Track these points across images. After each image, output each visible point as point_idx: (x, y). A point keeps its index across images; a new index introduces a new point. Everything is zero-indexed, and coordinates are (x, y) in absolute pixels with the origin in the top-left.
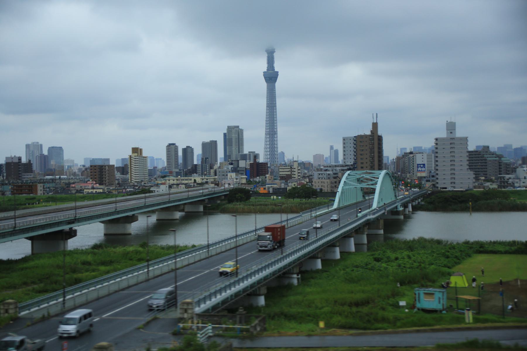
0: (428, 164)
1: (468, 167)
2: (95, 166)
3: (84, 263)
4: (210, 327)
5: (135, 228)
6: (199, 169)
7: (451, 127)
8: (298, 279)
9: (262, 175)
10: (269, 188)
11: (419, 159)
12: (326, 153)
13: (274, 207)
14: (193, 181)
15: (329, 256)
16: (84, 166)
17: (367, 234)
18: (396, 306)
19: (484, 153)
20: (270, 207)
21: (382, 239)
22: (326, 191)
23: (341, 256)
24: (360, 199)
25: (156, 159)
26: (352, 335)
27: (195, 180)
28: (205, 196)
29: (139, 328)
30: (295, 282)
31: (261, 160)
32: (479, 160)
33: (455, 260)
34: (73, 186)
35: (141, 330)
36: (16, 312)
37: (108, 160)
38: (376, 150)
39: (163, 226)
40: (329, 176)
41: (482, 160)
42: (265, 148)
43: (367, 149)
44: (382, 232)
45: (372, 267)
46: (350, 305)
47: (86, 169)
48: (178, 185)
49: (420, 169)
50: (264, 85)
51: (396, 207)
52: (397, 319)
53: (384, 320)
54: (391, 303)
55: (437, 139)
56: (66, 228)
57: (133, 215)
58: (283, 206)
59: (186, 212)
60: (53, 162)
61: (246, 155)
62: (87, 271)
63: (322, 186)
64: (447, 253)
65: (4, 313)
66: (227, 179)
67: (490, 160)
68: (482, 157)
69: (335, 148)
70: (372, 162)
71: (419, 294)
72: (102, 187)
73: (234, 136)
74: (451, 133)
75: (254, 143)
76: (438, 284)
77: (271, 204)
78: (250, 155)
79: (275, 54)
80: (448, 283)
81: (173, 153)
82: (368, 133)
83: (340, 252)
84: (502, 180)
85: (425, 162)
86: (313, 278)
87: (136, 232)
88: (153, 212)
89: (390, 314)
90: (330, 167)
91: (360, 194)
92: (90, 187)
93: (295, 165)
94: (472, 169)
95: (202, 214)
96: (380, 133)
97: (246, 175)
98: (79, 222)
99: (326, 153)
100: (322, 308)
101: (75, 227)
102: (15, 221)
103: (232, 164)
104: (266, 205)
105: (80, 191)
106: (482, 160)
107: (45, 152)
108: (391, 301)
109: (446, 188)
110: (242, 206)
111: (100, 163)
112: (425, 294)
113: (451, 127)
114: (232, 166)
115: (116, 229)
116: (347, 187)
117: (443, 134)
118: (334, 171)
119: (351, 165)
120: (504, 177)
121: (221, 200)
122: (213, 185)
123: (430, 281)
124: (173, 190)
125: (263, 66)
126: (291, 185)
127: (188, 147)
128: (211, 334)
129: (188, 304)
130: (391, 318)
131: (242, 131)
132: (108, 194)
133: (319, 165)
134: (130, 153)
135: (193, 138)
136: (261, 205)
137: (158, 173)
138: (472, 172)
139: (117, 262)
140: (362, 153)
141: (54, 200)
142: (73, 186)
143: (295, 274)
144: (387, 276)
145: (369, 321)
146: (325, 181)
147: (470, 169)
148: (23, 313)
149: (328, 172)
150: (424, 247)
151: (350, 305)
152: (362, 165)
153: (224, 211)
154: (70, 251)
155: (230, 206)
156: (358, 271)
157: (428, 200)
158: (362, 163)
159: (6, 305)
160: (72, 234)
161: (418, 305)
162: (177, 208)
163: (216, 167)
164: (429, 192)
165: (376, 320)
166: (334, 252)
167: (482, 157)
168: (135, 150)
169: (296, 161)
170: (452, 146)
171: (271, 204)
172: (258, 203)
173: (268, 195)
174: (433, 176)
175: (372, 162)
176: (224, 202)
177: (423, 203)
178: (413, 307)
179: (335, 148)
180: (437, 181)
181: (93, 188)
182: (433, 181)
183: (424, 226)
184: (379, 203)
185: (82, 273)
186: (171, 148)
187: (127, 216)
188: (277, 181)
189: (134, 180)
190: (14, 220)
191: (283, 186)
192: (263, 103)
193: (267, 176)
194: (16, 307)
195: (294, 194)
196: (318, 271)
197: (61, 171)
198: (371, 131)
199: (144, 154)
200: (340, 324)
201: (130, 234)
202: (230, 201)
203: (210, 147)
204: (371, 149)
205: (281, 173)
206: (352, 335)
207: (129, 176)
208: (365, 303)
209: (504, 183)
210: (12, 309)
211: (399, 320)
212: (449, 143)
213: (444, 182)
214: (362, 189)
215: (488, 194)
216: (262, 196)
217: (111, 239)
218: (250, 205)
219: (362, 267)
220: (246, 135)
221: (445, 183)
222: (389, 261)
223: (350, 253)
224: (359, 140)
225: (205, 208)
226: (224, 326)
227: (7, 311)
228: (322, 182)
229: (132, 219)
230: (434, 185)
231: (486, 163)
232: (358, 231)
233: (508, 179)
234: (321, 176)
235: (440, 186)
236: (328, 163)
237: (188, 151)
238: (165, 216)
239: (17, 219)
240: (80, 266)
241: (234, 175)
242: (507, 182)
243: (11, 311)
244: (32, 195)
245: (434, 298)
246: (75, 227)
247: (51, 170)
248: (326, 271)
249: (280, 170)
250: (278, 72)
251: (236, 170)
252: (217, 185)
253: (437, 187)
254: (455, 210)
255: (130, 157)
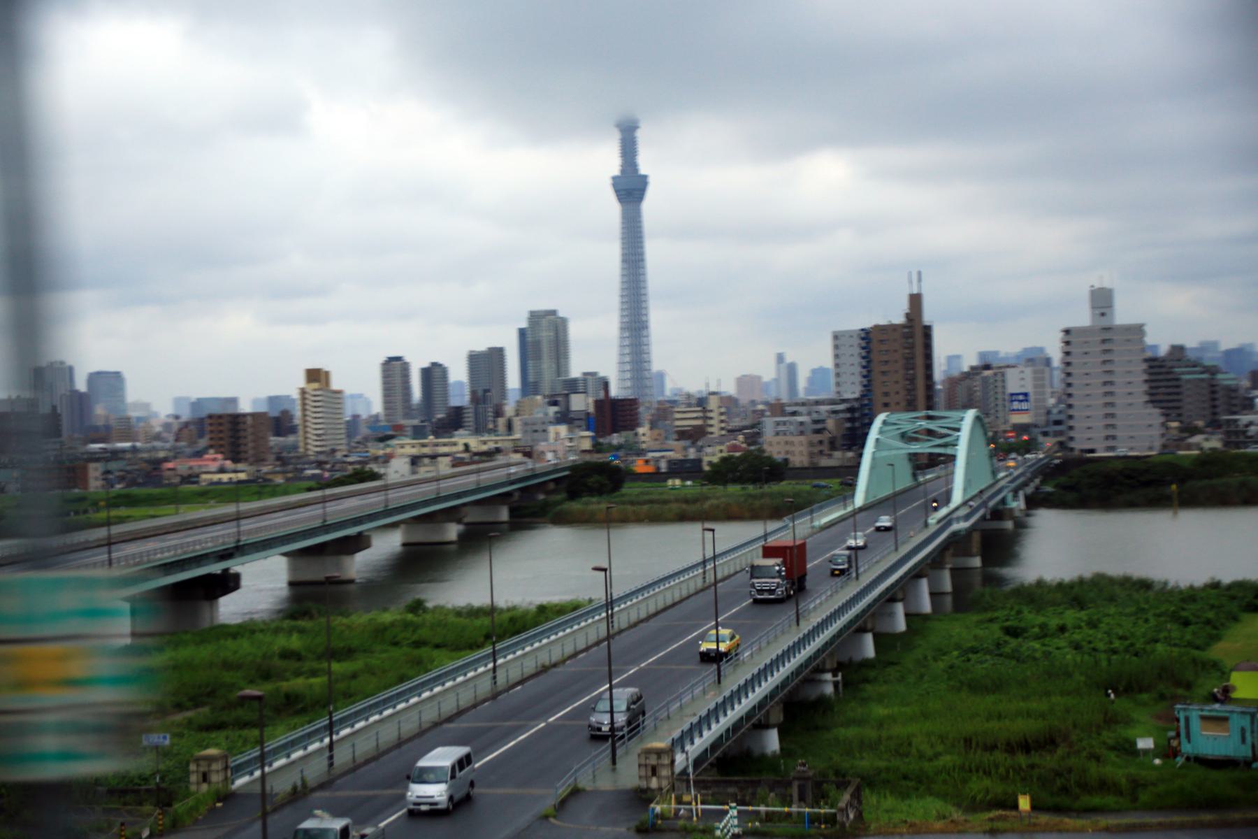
0: (1036, 393)
1: (1146, 398)
2: (220, 417)
3: (287, 655)
4: (735, 812)
5: (359, 565)
6: (469, 418)
7: (1102, 300)
8: (836, 684)
9: (625, 428)
10: (657, 460)
11: (1015, 382)
12: (768, 372)
13: (684, 506)
14: (461, 448)
15: (883, 627)
16: (177, 417)
17: (952, 569)
18: (1128, 749)
19: (1175, 363)
20: (674, 506)
21: (977, 579)
22: (798, 465)
23: (908, 625)
24: (905, 481)
25: (352, 396)
26: (1108, 829)
27: (466, 445)
28: (512, 483)
29: (546, 817)
30: (829, 689)
31: (614, 392)
32: (1170, 377)
33: (1208, 629)
34: (170, 465)
35: (552, 820)
36: (226, 779)
37: (233, 401)
38: (920, 361)
39: (420, 561)
40: (802, 428)
41: (1168, 380)
42: (622, 363)
43: (895, 359)
44: (977, 562)
45: (1014, 651)
46: (1010, 748)
47: (186, 424)
48: (434, 457)
49: (1016, 405)
50: (612, 209)
51: (1003, 501)
52: (1136, 785)
53: (1104, 786)
54: (1111, 742)
55: (1067, 332)
56: (216, 568)
57: (360, 534)
58: (707, 505)
59: (467, 524)
60: (100, 410)
61: (575, 381)
62: (298, 674)
63: (787, 452)
64: (1184, 614)
65: (198, 783)
66: (546, 440)
67: (1188, 381)
68: (1168, 373)
69: (788, 360)
70: (911, 390)
71: (1187, 719)
72: (240, 466)
73: (546, 335)
74: (1103, 314)
75: (594, 352)
76: (1202, 691)
77: (677, 500)
78: (585, 380)
79: (640, 135)
80: (1227, 690)
81: (398, 380)
82: (899, 319)
83: (907, 615)
84: (1232, 428)
85: (1029, 389)
86: (866, 680)
87: (367, 575)
88: (394, 525)
89: (1116, 770)
90: (803, 404)
91: (905, 470)
92: (214, 466)
93: (713, 404)
94: (1160, 401)
95: (506, 526)
96: (927, 318)
97: (588, 429)
98: (243, 555)
99: (768, 372)
100: (937, 756)
101: (235, 566)
102: (110, 553)
103: (555, 403)
104: (665, 502)
105: (191, 478)
106: (1168, 380)
107: (81, 385)
108: (1108, 736)
109: (1092, 451)
110: (603, 506)
111: (217, 410)
112: (1203, 718)
113: (1102, 300)
114: (555, 409)
115: (316, 571)
116: (884, 453)
117: (1082, 318)
118: (815, 416)
119: (856, 400)
120: (1236, 421)
121: (548, 493)
122: (517, 457)
123: (1178, 684)
124: (424, 471)
125: (612, 164)
126: (712, 455)
127: (435, 365)
128: (736, 830)
129: (659, 753)
130: (1124, 781)
131: (564, 321)
132: (259, 486)
133: (753, 403)
134: (301, 382)
135: (449, 338)
136: (651, 502)
137: (364, 431)
138: (1157, 411)
139: (365, 651)
140: (884, 368)
141: (131, 501)
142: (170, 465)
143: (828, 671)
144: (1069, 675)
145: (1065, 790)
146: (797, 439)
147: (1152, 402)
148: (240, 782)
149: (800, 419)
150: (1112, 599)
151: (1010, 748)
152: (886, 400)
153: (561, 520)
154: (224, 626)
155: (576, 506)
156: (981, 662)
157: (1063, 480)
158: (886, 394)
159: (202, 763)
160: (229, 583)
161: (1186, 748)
162: (451, 514)
163: (509, 409)
164: (1057, 461)
165: (1085, 787)
166: (892, 615)
167: (1168, 373)
168: (315, 375)
169: (714, 393)
170: (1107, 346)
171: (677, 500)
172: (647, 498)
173: (657, 477)
174: (1058, 423)
175: (911, 390)
176: (559, 497)
177: (1049, 489)
178: (1169, 752)
179: (788, 360)
180: (1072, 434)
181: (222, 470)
182: (1061, 433)
183: (1058, 547)
184: (965, 490)
185: (287, 680)
186: (394, 368)
187: (346, 538)
188: (671, 443)
189: (313, 449)
190: (105, 549)
191: (692, 454)
192: (612, 253)
193: (641, 430)
194: (226, 768)
195: (724, 472)
196: (866, 664)
197: (127, 429)
198: (907, 315)
199: (335, 386)
200: (989, 797)
201: (351, 581)
202: (573, 495)
203: (486, 364)
204: (907, 359)
205: (678, 423)
206: (1108, 829)
207: (301, 439)
208: (1048, 742)
209: (1237, 436)
210: (218, 771)
211: (1144, 786)
212: (1101, 340)
213: (1089, 436)
214: (913, 457)
215: (1209, 464)
216: (644, 481)
217: (309, 597)
218: (623, 503)
219: (988, 652)
220: (576, 332)
221: (1090, 437)
222: (1045, 636)
223: (925, 617)
224: (870, 339)
225: (513, 512)
226: (762, 808)
227: (205, 778)
228: (787, 443)
229: (358, 543)
230: (1061, 444)
231: (1178, 387)
232: (935, 562)
233: (1247, 426)
234: (781, 428)
235: (1078, 445)
236: (771, 396)
237: (434, 375)
238: (423, 535)
239: (114, 547)
240: (277, 662)
241: (563, 430)
242: (1244, 432)
243: (216, 778)
244: (76, 491)
245: (1228, 730)
246: (235, 566)
247: (96, 429)
248: (893, 664)
249: (678, 416)
250: (645, 177)
251: (565, 417)
252: (528, 454)
253: (1072, 449)
254: (1132, 505)
255: (303, 392)
